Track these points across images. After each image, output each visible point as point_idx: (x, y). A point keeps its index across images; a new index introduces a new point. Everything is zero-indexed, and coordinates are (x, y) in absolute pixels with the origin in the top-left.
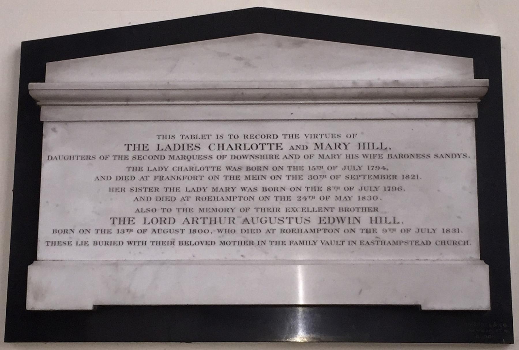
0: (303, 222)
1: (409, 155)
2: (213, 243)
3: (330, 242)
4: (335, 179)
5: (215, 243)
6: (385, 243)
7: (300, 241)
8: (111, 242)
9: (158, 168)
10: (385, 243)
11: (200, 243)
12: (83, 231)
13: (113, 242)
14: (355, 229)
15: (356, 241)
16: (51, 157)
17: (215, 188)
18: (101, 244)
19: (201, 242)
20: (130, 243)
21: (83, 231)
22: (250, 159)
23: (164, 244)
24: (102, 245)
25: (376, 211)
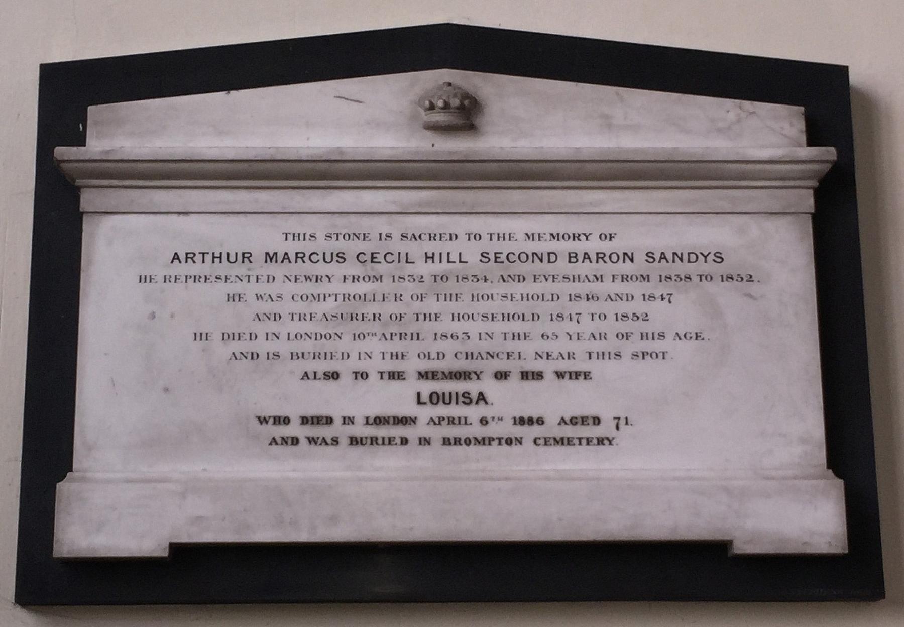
0: (480, 319)
1: (639, 277)
2: (295, 441)
3: (567, 354)
4: (470, 319)
5: (524, 279)
6: (579, 278)
7: (595, 276)
8: (304, 239)
9: (390, 335)
10: (579, 278)
11: (417, 237)
12: (301, 336)
13: (508, 233)
14: (371, 353)
15: (521, 438)
16: (557, 296)
17: (645, 277)
18: (364, 442)
19: (416, 239)
20: (560, 375)
21: (301, 336)
22: (380, 339)
23: (587, 377)
24: (366, 444)
25: (625, 280)
